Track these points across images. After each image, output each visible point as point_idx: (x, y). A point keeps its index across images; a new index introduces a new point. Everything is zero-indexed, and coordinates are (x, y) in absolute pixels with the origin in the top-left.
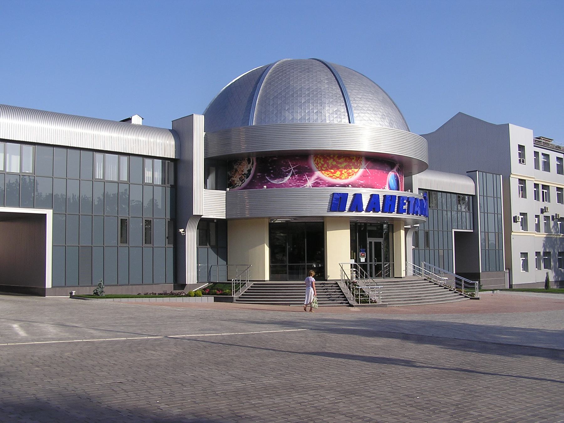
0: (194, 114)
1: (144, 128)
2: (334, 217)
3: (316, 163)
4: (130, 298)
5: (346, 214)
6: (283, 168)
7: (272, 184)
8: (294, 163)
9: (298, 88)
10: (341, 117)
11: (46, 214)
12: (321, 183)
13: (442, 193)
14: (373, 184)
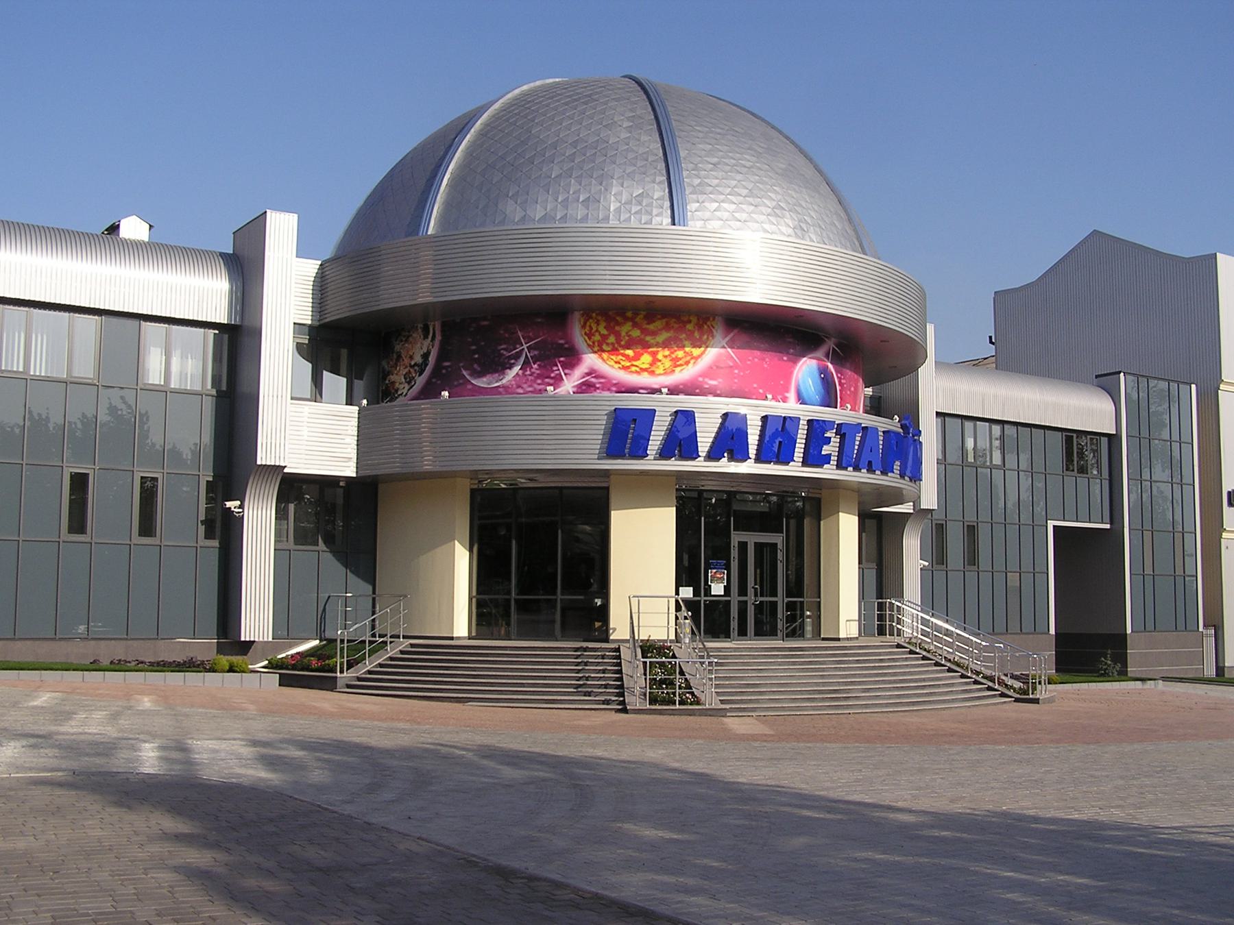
0: (267, 210)
1: (156, 250)
3: (586, 334)
5: (651, 463)
8: (531, 334)
10: (652, 210)
12: (598, 386)
13: (1019, 427)
14: (747, 390)
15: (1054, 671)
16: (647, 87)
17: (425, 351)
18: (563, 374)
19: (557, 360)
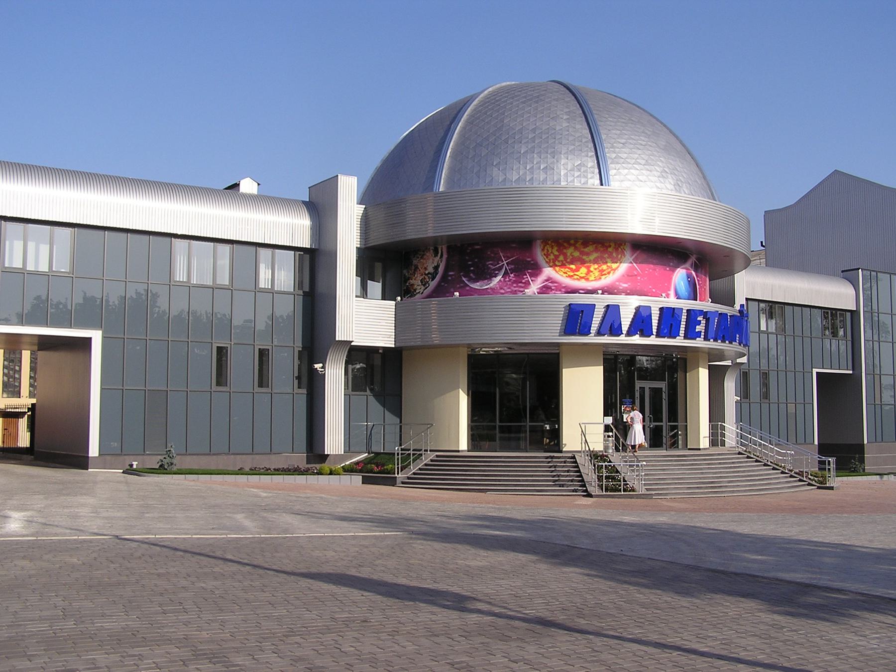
0: (339, 175)
1: (262, 200)
2: (591, 345)
3: (544, 254)
4: (215, 474)
5: (592, 339)
6: (490, 262)
7: (473, 290)
9: (517, 129)
10: (587, 175)
11: (91, 338)
12: (553, 288)
14: (645, 290)
15: (817, 469)
16: (573, 90)
17: (436, 265)
18: (530, 280)
19: (526, 272)
